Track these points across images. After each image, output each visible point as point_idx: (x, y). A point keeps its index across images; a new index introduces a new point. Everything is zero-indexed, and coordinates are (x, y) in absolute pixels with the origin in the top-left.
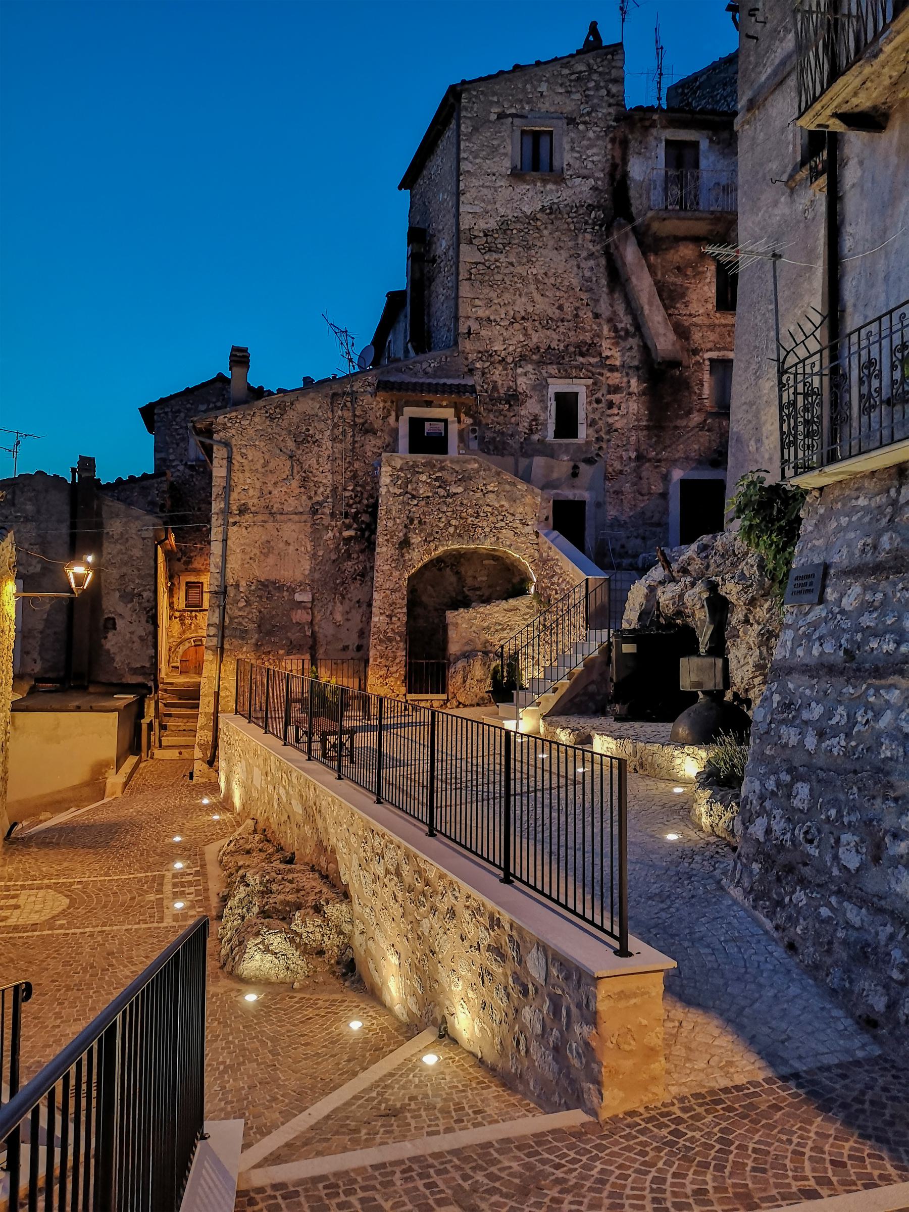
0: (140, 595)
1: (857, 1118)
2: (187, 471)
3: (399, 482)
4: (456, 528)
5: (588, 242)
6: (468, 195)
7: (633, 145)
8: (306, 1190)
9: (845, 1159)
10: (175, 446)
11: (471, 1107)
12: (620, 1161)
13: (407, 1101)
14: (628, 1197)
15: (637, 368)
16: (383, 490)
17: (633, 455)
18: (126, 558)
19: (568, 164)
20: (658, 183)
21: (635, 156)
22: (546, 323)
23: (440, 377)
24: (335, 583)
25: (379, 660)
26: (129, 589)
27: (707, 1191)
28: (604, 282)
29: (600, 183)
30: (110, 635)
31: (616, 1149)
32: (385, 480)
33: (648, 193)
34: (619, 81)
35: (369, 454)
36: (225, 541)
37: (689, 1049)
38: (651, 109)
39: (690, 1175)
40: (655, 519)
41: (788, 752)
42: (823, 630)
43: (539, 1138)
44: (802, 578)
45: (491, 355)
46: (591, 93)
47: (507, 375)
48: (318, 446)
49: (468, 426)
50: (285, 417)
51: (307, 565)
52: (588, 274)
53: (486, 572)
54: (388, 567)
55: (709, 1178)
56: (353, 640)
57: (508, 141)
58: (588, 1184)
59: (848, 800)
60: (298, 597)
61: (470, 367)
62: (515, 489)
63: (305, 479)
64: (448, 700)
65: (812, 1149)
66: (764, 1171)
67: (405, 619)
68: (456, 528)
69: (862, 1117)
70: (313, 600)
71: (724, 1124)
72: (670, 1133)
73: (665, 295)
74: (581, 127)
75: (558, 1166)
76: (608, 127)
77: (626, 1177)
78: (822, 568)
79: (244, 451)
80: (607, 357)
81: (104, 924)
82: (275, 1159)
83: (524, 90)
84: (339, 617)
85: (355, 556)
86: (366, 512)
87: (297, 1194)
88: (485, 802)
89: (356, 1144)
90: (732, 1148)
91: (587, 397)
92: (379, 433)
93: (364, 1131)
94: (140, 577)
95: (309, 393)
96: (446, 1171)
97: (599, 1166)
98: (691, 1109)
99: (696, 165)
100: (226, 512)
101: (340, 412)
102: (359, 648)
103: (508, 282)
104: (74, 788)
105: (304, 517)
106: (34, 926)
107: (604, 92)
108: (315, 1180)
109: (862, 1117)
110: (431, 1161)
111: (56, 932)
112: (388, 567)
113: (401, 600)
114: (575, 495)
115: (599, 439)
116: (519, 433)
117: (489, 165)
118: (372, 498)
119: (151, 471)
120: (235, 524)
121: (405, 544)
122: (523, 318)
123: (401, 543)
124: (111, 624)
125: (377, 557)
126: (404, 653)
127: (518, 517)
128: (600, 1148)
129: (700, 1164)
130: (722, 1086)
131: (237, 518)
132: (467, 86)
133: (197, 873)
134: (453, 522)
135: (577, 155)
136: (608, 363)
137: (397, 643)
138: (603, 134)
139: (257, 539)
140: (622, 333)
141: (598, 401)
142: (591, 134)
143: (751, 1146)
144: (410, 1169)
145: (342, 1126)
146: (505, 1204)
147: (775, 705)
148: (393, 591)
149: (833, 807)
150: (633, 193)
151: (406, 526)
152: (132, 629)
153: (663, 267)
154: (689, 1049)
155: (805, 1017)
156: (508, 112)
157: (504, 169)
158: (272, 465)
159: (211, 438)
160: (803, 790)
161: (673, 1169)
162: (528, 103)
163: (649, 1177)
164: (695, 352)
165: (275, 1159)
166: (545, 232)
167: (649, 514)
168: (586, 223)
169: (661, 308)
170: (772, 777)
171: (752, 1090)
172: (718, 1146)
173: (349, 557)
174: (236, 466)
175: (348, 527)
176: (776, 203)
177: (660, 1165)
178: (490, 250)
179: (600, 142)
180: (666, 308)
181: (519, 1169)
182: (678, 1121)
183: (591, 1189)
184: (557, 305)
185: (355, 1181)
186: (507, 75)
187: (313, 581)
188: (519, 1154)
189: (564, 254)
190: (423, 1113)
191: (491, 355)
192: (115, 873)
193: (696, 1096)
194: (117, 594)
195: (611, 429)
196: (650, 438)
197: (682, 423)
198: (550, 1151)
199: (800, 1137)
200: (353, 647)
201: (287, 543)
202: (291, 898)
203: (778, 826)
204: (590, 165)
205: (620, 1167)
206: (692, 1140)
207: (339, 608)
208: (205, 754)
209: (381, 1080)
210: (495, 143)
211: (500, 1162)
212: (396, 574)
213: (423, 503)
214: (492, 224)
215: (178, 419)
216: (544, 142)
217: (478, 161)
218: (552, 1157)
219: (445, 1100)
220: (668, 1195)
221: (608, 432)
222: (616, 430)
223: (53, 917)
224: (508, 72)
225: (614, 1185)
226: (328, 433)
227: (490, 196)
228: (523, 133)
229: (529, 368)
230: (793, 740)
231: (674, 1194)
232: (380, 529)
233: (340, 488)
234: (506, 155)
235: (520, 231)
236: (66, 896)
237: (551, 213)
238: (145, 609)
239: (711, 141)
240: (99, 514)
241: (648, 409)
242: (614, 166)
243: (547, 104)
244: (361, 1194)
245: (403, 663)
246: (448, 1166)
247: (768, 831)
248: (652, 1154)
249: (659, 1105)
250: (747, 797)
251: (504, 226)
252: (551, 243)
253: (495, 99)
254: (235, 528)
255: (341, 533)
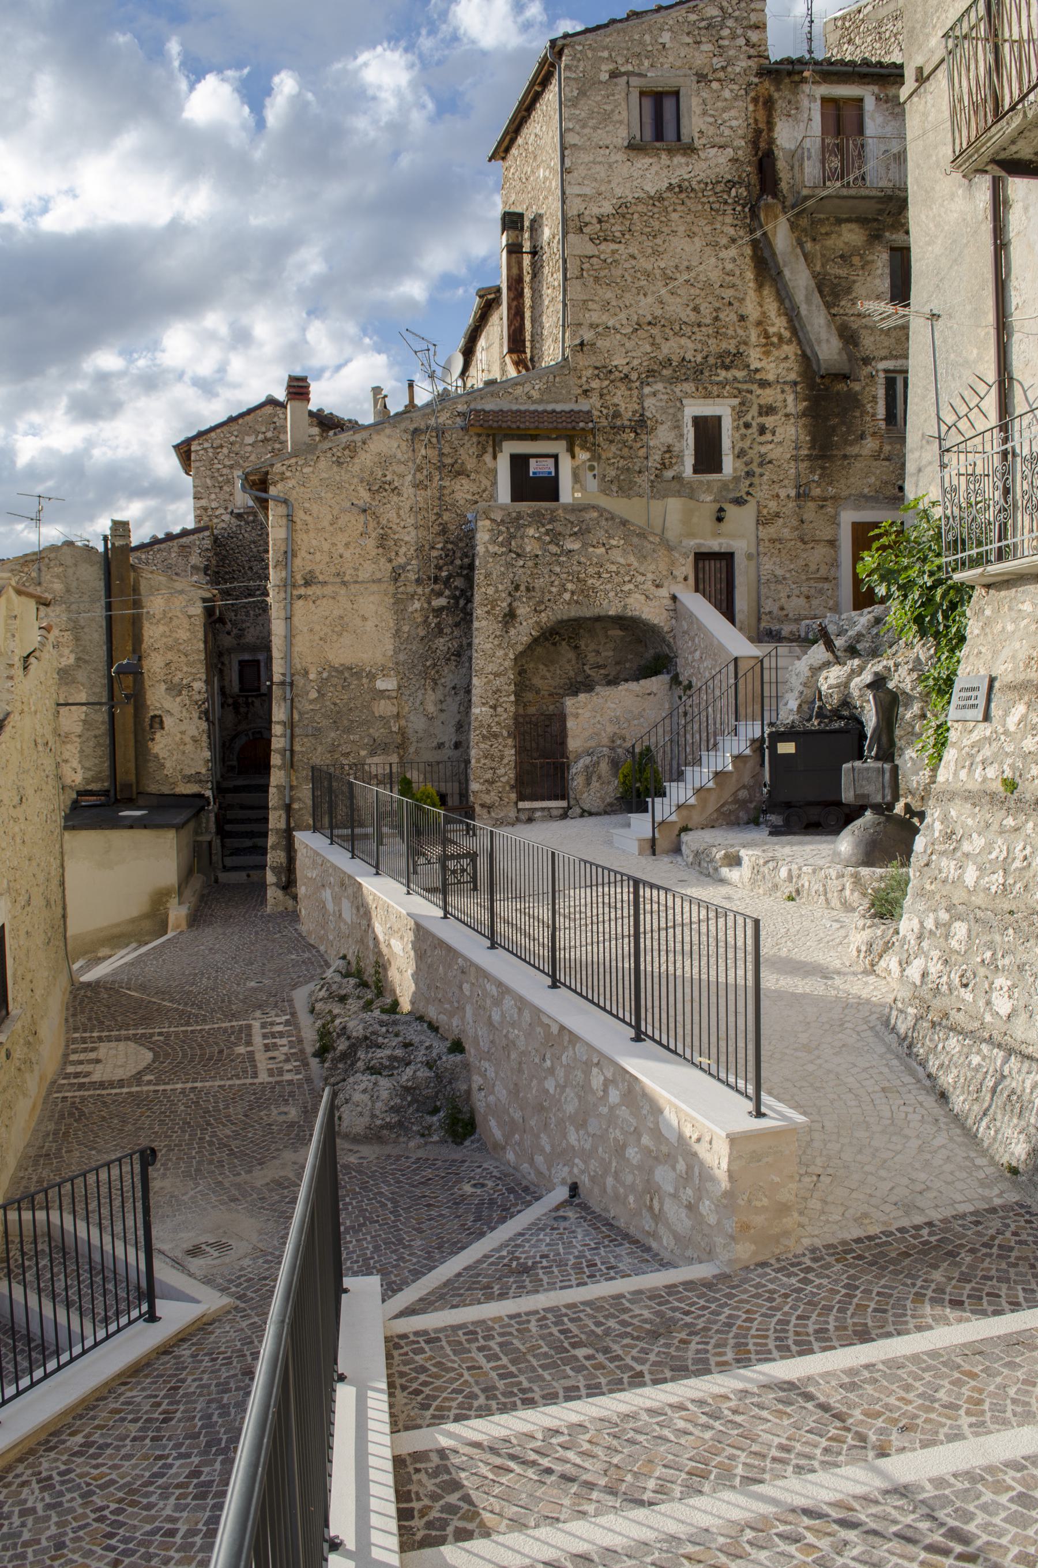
0: (189, 686)
1: (983, 1261)
2: (233, 520)
3: (500, 539)
4: (573, 593)
5: (727, 226)
6: (575, 174)
7: (780, 104)
8: (447, 1336)
9: (964, 1298)
10: (217, 490)
11: (603, 1263)
12: (748, 1307)
13: (538, 1259)
14: (753, 1337)
15: (795, 384)
16: (480, 549)
17: (793, 493)
18: (170, 641)
19: (701, 132)
20: (813, 151)
21: (784, 118)
22: (677, 328)
23: (549, 402)
24: (424, 665)
25: (483, 761)
26: (176, 680)
27: (827, 1330)
28: (750, 275)
29: (740, 152)
30: (158, 736)
31: (745, 1297)
32: (482, 537)
33: (801, 165)
34: (760, 27)
35: (462, 502)
36: (289, 618)
37: (825, 1202)
38: (800, 61)
39: (814, 1316)
40: (823, 572)
41: (948, 887)
42: (987, 752)
43: (671, 1289)
44: (967, 690)
45: (610, 372)
46: (726, 43)
47: (631, 396)
48: (399, 494)
49: (584, 462)
50: (356, 460)
51: (389, 645)
52: (730, 266)
53: (612, 645)
54: (490, 645)
55: (831, 1319)
56: (448, 736)
57: (624, 105)
58: (715, 1327)
59: (1003, 942)
60: (381, 684)
61: (585, 387)
62: (646, 544)
63: (383, 537)
64: (569, 808)
65: (934, 1291)
66: (885, 1311)
67: (513, 709)
68: (573, 593)
69: (988, 1260)
70: (399, 688)
71: (852, 1272)
72: (799, 1281)
73: (826, 290)
74: (715, 85)
75: (687, 1313)
76: (749, 84)
77: (751, 1320)
78: (987, 680)
79: (307, 505)
80: (757, 370)
81: (195, 1080)
82: (409, 1312)
83: (641, 43)
84: (431, 708)
85: (447, 630)
86: (459, 575)
87: (438, 1339)
88: (620, 921)
89: (489, 1298)
90: (858, 1292)
91: (734, 420)
92: (473, 476)
93: (496, 1287)
94: (189, 664)
95: (383, 430)
96: (579, 1319)
97: (727, 1311)
98: (822, 1258)
99: (861, 130)
100: (290, 584)
101: (423, 452)
102: (457, 745)
103: (629, 279)
104: (133, 921)
105: (384, 586)
106: (121, 1083)
107: (741, 41)
108: (455, 1328)
109: (988, 1260)
110: (564, 1311)
111: (145, 1088)
112: (490, 645)
113: (506, 684)
114: (720, 544)
115: (749, 474)
116: (647, 468)
117: (601, 136)
118: (467, 556)
119: (190, 525)
120: (300, 597)
121: (510, 616)
122: (650, 323)
123: (505, 615)
124: (157, 721)
125: (475, 633)
126: (513, 752)
127: (650, 576)
128: (730, 1296)
129: (824, 1308)
130: (855, 1236)
131: (302, 591)
132: (569, 40)
133: (287, 1023)
134: (570, 586)
135: (712, 120)
136: (758, 377)
137: (504, 739)
138: (743, 92)
139: (327, 613)
140: (775, 340)
141: (747, 426)
142: (727, 94)
143: (876, 1290)
144: (544, 1318)
145: (474, 1283)
146: (636, 1346)
147: (937, 834)
148: (496, 675)
149: (989, 949)
150: (781, 165)
151: (510, 594)
152: (183, 728)
153: (823, 256)
154: (825, 1202)
155: (948, 1167)
156: (623, 69)
157: (620, 140)
158: (341, 523)
159: (265, 490)
160: (960, 929)
161: (799, 1312)
162: (647, 58)
163: (775, 1320)
164: (867, 361)
165: (409, 1312)
166: (674, 216)
167: (813, 567)
168: (726, 203)
169: (823, 307)
170: (931, 915)
171: (884, 1239)
172: (844, 1291)
173: (441, 632)
174: (299, 526)
175: (440, 594)
176: (953, 196)
177: (786, 1309)
178: (605, 240)
179: (740, 104)
180: (828, 306)
181: (651, 1316)
182: (808, 1270)
183: (718, 1331)
184: (692, 305)
185: (493, 1329)
186: (619, 25)
187: (397, 663)
188: (649, 1303)
189: (698, 242)
190: (555, 1270)
191: (610, 372)
192: (197, 1023)
193: (828, 1247)
194: (163, 687)
195: (764, 461)
196: (812, 471)
197: (853, 450)
198: (680, 1300)
199: (925, 1281)
200: (450, 743)
201: (364, 619)
202: (399, 1052)
203: (934, 968)
204: (727, 132)
205: (747, 1312)
206: (819, 1287)
207: (431, 697)
208: (279, 879)
209: (511, 1239)
210: (608, 108)
211: (631, 1310)
212: (500, 653)
213: (530, 564)
214: (607, 208)
215: (220, 457)
216: (668, 104)
217: (587, 131)
218: (682, 1305)
219: (576, 1257)
220: (791, 1334)
221: (761, 465)
222: (770, 462)
223: (139, 1073)
224: (621, 21)
225: (740, 1327)
226: (409, 478)
227: (603, 174)
228: (642, 94)
229: (659, 386)
230: (953, 874)
231: (797, 1333)
232: (477, 598)
233: (427, 547)
234: (621, 122)
235: (642, 215)
236: (150, 1049)
237: (681, 192)
238: (196, 703)
239: (878, 99)
240: (136, 590)
241: (810, 433)
242: (758, 132)
243: (671, 59)
244: (499, 1339)
245: (513, 764)
246: (582, 1315)
247: (924, 975)
248: (779, 1300)
249: (790, 1256)
250: (905, 937)
251: (622, 210)
252: (681, 229)
253: (606, 54)
254: (301, 602)
255: (429, 603)
